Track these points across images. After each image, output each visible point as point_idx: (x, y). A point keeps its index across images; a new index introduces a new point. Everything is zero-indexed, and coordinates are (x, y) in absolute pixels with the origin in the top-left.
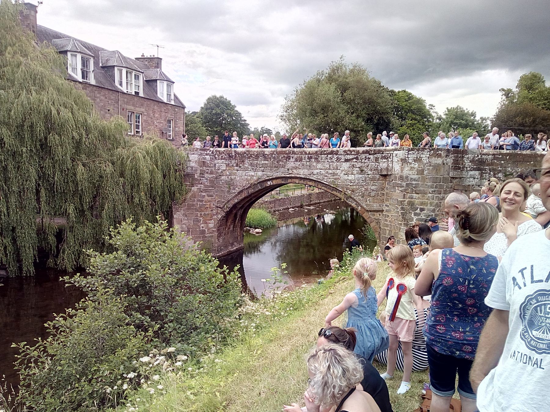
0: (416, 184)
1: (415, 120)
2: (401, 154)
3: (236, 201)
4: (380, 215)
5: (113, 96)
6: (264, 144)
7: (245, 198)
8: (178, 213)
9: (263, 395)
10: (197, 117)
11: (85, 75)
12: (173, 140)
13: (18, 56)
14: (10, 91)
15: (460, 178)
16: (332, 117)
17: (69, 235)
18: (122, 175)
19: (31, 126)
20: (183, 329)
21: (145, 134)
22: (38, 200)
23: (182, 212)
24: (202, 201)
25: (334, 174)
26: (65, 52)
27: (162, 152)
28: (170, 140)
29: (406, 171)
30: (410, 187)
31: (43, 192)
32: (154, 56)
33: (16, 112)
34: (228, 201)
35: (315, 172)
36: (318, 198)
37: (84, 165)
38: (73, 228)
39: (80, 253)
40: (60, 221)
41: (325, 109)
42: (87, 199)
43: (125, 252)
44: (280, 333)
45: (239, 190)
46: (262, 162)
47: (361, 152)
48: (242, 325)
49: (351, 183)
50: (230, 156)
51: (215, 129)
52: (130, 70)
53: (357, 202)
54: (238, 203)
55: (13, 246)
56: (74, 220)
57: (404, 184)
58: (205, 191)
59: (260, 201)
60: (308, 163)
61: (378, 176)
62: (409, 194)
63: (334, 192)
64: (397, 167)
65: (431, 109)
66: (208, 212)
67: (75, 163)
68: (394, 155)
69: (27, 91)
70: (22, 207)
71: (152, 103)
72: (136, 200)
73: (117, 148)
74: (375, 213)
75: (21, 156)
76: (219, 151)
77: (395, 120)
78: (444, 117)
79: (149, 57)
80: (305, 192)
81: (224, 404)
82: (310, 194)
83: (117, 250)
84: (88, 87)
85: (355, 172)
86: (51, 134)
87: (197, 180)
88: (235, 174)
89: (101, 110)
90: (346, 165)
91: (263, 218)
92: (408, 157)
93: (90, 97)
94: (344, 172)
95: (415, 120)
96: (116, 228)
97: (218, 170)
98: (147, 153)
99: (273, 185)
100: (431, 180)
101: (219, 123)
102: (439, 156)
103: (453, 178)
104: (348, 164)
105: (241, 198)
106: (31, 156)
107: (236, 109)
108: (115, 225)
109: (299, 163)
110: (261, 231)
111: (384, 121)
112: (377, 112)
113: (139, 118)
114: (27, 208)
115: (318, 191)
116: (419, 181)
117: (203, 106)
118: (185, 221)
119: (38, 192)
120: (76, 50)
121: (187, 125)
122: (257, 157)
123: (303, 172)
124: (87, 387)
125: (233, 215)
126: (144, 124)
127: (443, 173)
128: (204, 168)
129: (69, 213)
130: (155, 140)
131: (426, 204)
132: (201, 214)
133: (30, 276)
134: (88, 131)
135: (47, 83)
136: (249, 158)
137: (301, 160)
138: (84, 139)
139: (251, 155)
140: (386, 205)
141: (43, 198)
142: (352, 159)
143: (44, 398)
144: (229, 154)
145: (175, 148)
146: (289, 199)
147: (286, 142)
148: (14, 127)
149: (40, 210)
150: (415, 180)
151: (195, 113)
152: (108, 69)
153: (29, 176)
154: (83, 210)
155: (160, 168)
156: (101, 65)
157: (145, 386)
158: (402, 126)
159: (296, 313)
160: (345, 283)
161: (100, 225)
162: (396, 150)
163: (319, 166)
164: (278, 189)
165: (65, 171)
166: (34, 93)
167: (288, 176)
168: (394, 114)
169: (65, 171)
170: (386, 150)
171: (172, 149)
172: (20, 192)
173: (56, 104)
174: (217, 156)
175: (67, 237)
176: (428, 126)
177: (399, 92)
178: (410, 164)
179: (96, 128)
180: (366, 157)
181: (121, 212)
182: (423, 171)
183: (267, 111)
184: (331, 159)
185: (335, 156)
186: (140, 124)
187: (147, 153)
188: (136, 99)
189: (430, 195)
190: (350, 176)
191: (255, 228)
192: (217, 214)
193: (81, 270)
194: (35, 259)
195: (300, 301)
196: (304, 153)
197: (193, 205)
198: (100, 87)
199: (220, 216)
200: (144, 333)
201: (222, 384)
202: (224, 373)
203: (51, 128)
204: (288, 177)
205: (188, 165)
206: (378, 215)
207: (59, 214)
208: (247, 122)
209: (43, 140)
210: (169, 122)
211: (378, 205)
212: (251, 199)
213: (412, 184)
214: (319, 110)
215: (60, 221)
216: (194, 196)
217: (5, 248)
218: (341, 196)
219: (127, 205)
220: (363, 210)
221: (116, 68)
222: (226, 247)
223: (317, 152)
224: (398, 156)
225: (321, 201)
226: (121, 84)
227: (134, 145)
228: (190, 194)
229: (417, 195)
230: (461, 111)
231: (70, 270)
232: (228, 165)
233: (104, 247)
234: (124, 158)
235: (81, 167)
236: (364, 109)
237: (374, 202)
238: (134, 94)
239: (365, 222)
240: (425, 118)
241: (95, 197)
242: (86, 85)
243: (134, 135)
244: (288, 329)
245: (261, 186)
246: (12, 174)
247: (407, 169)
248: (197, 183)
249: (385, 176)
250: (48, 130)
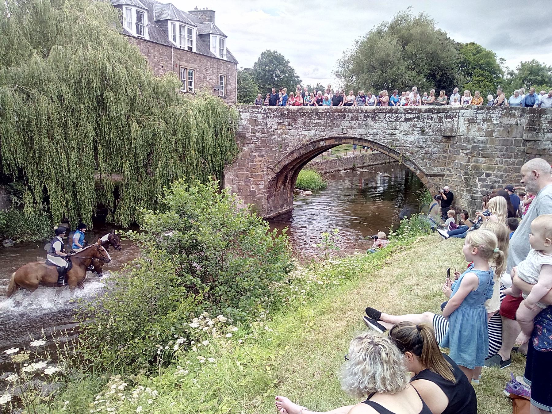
0: (483, 147)
1: (483, 76)
2: (469, 113)
3: (287, 162)
4: (440, 180)
5: (167, 52)
6: (319, 102)
7: (296, 159)
8: (229, 173)
9: (318, 378)
10: (249, 74)
11: (139, 29)
12: (225, 98)
13: (75, 10)
14: (68, 47)
15: (535, 141)
16: (390, 73)
17: (124, 192)
18: (174, 133)
19: (88, 83)
20: (233, 293)
21: (198, 91)
22: (96, 157)
23: (233, 172)
24: (252, 161)
25: (392, 135)
26: (120, 6)
27: (213, 110)
28: (222, 98)
29: (473, 132)
30: (477, 151)
31: (100, 149)
32: (207, 8)
33: (74, 68)
34: (279, 162)
35: (372, 132)
36: (371, 160)
37: (138, 123)
38: (128, 184)
39: (135, 210)
40: (117, 177)
41: (384, 64)
42: (141, 157)
43: (178, 212)
44: (333, 304)
45: (290, 151)
46: (316, 121)
47: (423, 110)
48: (292, 291)
49: (411, 144)
50: (282, 114)
51: (268, 87)
52: (183, 24)
53: (416, 165)
54: (289, 164)
55: (74, 200)
56: (129, 177)
57: (470, 146)
58: (256, 151)
59: (311, 162)
60: (364, 123)
61: (440, 138)
62: (474, 158)
63: (391, 155)
64: (462, 128)
65: (502, 63)
66: (259, 172)
67: (130, 120)
68: (460, 114)
69: (83, 46)
70: (81, 164)
71: (205, 59)
72: (188, 158)
73: (170, 105)
74: (435, 178)
75: (79, 112)
76: (271, 109)
77: (460, 77)
78: (516, 72)
79: (202, 9)
80: (358, 153)
81: (274, 382)
82: (363, 156)
83: (169, 208)
84: (142, 42)
85: (415, 133)
86: (107, 91)
87: (248, 139)
88: (287, 134)
89: (155, 66)
90: (406, 125)
91: (313, 180)
92: (476, 117)
93: (144, 52)
94: (403, 133)
95: (483, 76)
96: (169, 188)
97: (270, 129)
98: (199, 110)
99: (326, 146)
100: (501, 142)
101: (272, 81)
102: (513, 116)
103: (527, 140)
105: (292, 159)
106: (89, 113)
107: (289, 65)
108: (168, 183)
109: (355, 122)
110: (311, 193)
111: (448, 78)
112: (440, 68)
113: (192, 75)
114: (86, 164)
115: (372, 153)
116: (487, 144)
117: (257, 61)
118: (235, 182)
119: (96, 149)
120: (130, 3)
121: (239, 82)
122: (310, 115)
123: (358, 132)
124: (141, 345)
125: (284, 177)
126: (196, 81)
127: (516, 134)
128: (256, 127)
129: (124, 171)
130: (208, 98)
131: (493, 169)
132: (251, 175)
133: (89, 230)
134: (142, 87)
135: (102, 38)
136: (302, 116)
137: (357, 119)
138: (138, 97)
139: (304, 113)
140: (448, 169)
141: (100, 156)
142: (413, 118)
143: (100, 352)
144: (281, 113)
145: (226, 105)
146: (340, 160)
147: (338, 99)
148: (72, 83)
149: (98, 167)
150: (482, 142)
151: (247, 69)
152: (161, 24)
153: (87, 133)
154: (138, 167)
155: (212, 126)
156: (155, 19)
157: (194, 348)
158: (467, 83)
159: (350, 283)
160: (403, 254)
161: (154, 183)
162: (463, 108)
163: (377, 125)
164: (330, 150)
165: (120, 128)
166: (90, 48)
167: (342, 136)
168: (459, 69)
169: (120, 128)
170: (451, 109)
171: (224, 107)
172: (79, 149)
173: (111, 60)
174: (268, 114)
175: (123, 194)
176: (497, 83)
177: (467, 45)
178: (479, 124)
179: (150, 84)
180: (428, 116)
181: (174, 170)
182: (492, 132)
183: (320, 67)
184: (390, 117)
185: (395, 115)
186: (193, 81)
187: (199, 110)
188: (189, 55)
189: (498, 159)
190: (409, 136)
191: (305, 190)
192: (268, 174)
193: (135, 226)
194: (94, 214)
195: (354, 270)
197: (244, 165)
198: (153, 42)
199: (270, 177)
200: (194, 296)
201: (273, 357)
202: (274, 344)
203: (107, 85)
204: (343, 138)
205: (240, 124)
206: (439, 180)
207: (116, 171)
208: (300, 79)
209: (99, 97)
210: (221, 78)
211: (439, 169)
212: (303, 160)
213: (479, 147)
214: (377, 65)
215: (117, 177)
216: (245, 156)
217: (67, 202)
218: (399, 158)
219: (179, 164)
220: (422, 174)
221: (169, 22)
222: (276, 208)
223: (374, 110)
224: (465, 115)
225: (374, 163)
226: (174, 39)
227: (186, 102)
228: (241, 154)
229: (484, 159)
230: (538, 66)
231: (126, 226)
232: (279, 124)
233: (157, 206)
234: (176, 115)
235: (135, 125)
236: (426, 64)
237: (434, 166)
238: (187, 49)
239: (422, 185)
240: (494, 74)
241: (149, 155)
242: (140, 40)
243: (187, 92)
244: (342, 301)
245: (313, 146)
246: (72, 130)
247: (474, 130)
248: (248, 142)
249: (448, 138)
250: (104, 87)
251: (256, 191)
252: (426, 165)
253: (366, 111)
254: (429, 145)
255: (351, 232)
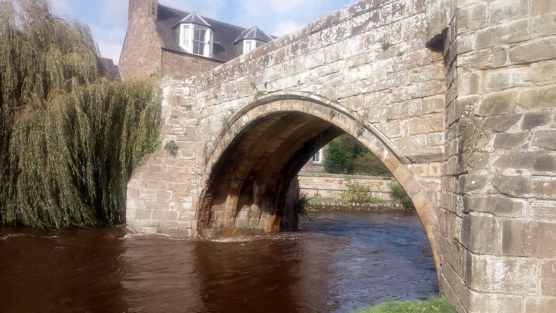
0: (512, 29)
25: (333, 73)
49: (365, 86)
62: (490, 74)
85: (372, 56)
90: (353, 45)
104: (358, 39)
128: (179, 107)
132: (170, 185)
142: (367, 22)
163: (309, 61)
196: (286, 41)
197: (158, 169)
213: (498, 33)
251: (178, 213)
252: (398, 131)
253: (294, 37)
254: (401, 77)
255: (167, 284)
